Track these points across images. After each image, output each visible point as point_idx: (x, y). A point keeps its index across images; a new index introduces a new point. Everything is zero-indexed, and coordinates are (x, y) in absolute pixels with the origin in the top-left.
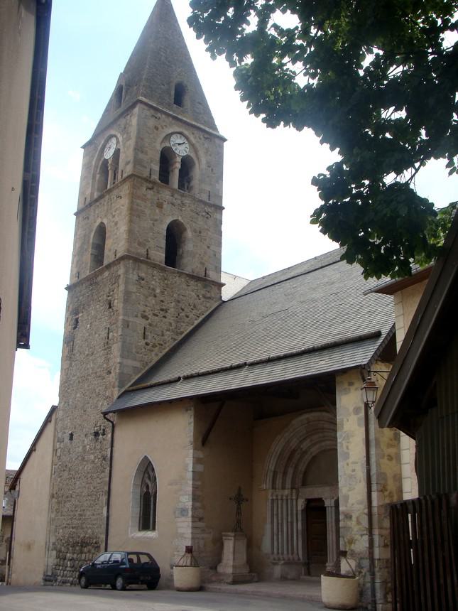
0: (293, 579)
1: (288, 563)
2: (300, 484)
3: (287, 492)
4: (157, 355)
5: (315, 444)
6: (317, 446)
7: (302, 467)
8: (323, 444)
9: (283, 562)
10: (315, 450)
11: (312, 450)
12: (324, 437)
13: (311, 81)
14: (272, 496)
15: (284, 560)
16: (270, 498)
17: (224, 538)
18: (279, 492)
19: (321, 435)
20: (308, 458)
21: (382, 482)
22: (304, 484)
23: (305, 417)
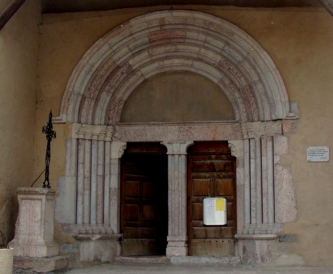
0: (108, 263)
1: (105, 238)
2: (118, 119)
3: (98, 130)
4: (247, 158)
5: (152, 62)
6: (155, 65)
7: (123, 94)
8: (167, 62)
9: (98, 236)
10: (150, 70)
11: (143, 71)
12: (176, 51)
13: (117, 243)
14: (77, 133)
15: (100, 233)
16: (74, 136)
17: (20, 197)
18: (89, 129)
19: (173, 48)
20: (135, 81)
21: (220, 232)
22: (123, 121)
23: (155, 17)
